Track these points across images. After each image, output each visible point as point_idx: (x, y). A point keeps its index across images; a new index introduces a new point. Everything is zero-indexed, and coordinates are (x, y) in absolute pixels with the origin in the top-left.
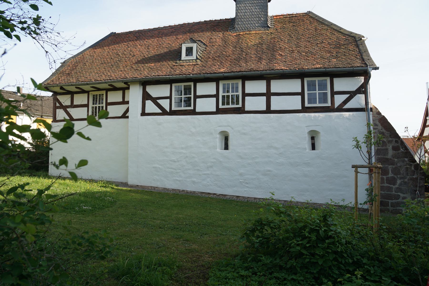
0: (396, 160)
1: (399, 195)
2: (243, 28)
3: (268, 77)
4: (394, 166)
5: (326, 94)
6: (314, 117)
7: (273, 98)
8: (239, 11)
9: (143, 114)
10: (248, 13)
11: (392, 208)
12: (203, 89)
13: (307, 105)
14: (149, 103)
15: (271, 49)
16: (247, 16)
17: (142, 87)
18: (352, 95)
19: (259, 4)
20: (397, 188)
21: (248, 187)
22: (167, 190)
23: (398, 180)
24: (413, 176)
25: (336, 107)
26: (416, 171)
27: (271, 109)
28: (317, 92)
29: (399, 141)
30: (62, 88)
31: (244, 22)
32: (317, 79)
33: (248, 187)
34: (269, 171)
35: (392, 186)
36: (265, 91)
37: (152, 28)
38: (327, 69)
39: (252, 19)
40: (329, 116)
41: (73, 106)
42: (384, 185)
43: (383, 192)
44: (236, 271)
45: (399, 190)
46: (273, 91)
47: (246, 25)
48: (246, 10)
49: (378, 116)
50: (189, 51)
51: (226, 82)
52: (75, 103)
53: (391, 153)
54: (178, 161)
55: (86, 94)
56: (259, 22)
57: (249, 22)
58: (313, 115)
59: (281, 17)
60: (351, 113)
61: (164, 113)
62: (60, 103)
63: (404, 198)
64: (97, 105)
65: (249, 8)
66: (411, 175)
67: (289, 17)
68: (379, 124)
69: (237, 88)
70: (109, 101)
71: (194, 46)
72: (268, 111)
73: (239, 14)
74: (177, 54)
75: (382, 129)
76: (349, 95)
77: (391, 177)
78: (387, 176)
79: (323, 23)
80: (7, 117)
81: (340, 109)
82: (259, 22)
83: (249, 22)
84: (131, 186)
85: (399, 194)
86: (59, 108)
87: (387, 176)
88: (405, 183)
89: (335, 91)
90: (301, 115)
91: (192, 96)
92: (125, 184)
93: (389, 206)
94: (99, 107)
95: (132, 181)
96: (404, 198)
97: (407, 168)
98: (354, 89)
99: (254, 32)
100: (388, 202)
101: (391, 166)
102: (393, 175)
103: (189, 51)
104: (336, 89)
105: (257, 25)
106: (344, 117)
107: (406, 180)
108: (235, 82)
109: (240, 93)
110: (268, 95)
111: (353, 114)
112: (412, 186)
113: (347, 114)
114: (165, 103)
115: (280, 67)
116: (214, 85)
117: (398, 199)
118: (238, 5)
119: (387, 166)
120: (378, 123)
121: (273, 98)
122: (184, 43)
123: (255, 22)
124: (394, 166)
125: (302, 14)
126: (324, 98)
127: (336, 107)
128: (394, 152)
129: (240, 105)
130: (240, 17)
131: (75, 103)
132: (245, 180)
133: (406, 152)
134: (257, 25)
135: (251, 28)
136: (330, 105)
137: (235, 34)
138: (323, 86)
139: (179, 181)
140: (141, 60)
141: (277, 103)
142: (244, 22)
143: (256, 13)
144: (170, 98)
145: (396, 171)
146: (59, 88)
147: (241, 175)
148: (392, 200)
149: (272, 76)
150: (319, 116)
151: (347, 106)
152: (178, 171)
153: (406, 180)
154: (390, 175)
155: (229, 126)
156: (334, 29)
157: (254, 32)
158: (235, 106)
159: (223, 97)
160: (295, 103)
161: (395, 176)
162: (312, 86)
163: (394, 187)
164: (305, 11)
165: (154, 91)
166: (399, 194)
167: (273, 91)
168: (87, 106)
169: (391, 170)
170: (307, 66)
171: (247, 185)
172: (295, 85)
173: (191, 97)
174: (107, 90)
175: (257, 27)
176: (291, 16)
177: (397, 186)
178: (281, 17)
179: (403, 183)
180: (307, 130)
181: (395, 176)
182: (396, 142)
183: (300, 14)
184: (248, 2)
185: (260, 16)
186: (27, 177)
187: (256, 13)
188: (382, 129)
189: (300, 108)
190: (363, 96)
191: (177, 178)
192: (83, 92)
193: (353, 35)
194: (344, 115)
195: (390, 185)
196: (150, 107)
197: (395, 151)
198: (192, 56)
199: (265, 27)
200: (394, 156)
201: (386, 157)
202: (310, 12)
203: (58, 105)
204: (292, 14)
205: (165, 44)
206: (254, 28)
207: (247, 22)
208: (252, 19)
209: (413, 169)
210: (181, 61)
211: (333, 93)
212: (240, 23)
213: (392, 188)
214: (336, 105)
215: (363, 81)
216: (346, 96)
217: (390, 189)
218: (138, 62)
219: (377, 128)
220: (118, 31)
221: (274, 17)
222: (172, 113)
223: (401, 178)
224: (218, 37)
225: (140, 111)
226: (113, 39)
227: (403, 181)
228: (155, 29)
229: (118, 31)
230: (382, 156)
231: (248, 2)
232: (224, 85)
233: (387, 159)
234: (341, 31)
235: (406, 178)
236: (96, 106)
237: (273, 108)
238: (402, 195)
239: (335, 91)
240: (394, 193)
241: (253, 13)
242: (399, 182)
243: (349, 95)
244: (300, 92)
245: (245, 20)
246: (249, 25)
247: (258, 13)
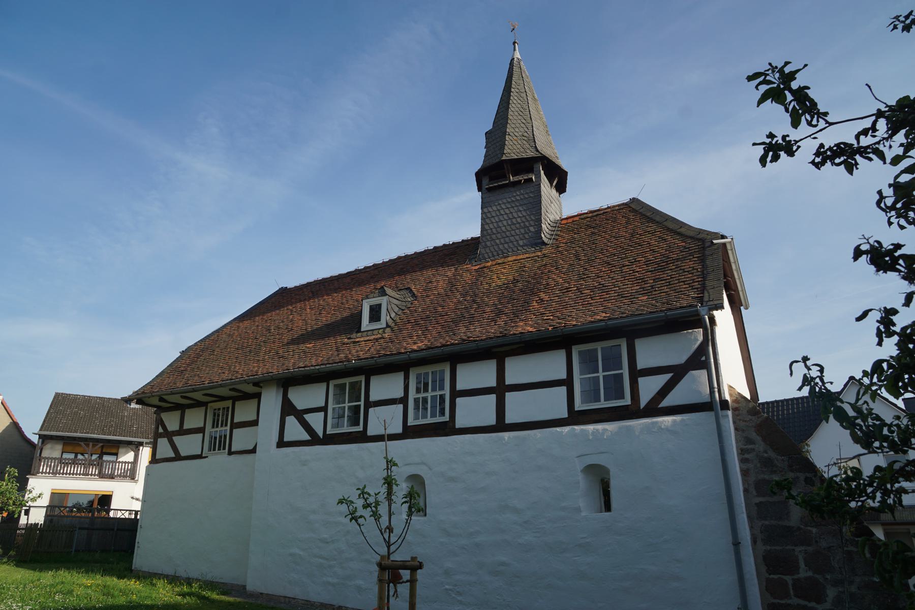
0: (814, 530)
2: (495, 253)
3: (497, 351)
6: (593, 432)
7: (509, 396)
8: (488, 221)
9: (281, 444)
12: (385, 387)
13: (579, 406)
14: (291, 420)
15: (525, 291)
16: (503, 228)
17: (282, 390)
18: (678, 373)
19: (525, 202)
25: (642, 407)
27: (457, 427)
28: (601, 374)
31: (498, 241)
32: (599, 346)
34: (503, 564)
35: (813, 604)
36: (493, 383)
37: (345, 272)
38: (610, 323)
40: (629, 428)
41: (182, 432)
42: (789, 602)
47: (501, 246)
48: (501, 218)
49: (753, 418)
50: (375, 314)
51: (422, 370)
53: (796, 514)
56: (526, 236)
57: (507, 239)
58: (590, 428)
59: (577, 219)
60: (678, 418)
61: (315, 440)
65: (507, 212)
67: (591, 217)
68: (759, 438)
69: (442, 380)
70: (460, 386)
71: (384, 301)
72: (501, 426)
74: (352, 323)
75: (766, 452)
78: (796, 577)
79: (650, 220)
81: (653, 409)
82: (526, 236)
83: (507, 239)
84: (252, 595)
87: (796, 577)
89: (639, 368)
90: (566, 429)
91: (362, 403)
92: (241, 590)
95: (253, 585)
98: (681, 358)
99: (514, 258)
101: (803, 548)
102: (810, 574)
103: (375, 314)
104: (641, 364)
105: (521, 243)
106: (660, 427)
107: (853, 589)
108: (437, 368)
109: (447, 392)
110: (501, 390)
111: (683, 420)
113: (667, 420)
114: (316, 421)
115: (526, 327)
116: (399, 378)
118: (486, 210)
119: (789, 547)
120: (754, 435)
121: (509, 396)
122: (367, 297)
123: (517, 237)
124: (810, 549)
125: (619, 205)
129: (446, 418)
131: (186, 426)
132: (456, 585)
136: (629, 403)
138: (612, 361)
140: (298, 338)
141: (518, 407)
143: (519, 220)
150: (605, 430)
151: (666, 402)
154: (804, 573)
155: (423, 463)
156: (668, 229)
157: (514, 258)
158: (439, 419)
159: (416, 401)
160: (553, 403)
162: (589, 362)
164: (625, 199)
165: (303, 398)
168: (201, 430)
170: (577, 318)
172: (552, 365)
173: (360, 405)
174: (235, 400)
175: (522, 246)
178: (577, 219)
180: (579, 466)
182: (808, 481)
183: (614, 206)
184: (505, 201)
185: (527, 224)
188: (766, 452)
189: (564, 414)
190: (704, 373)
191: (330, 579)
193: (700, 236)
194: (662, 422)
195: (806, 603)
196: (294, 430)
198: (383, 319)
199: (536, 245)
202: (634, 200)
205: (351, 302)
206: (515, 249)
208: (513, 232)
209: (868, 555)
210: (359, 334)
211: (636, 374)
212: (488, 243)
215: (701, 338)
216: (664, 378)
219: (753, 450)
220: (291, 284)
221: (564, 222)
224: (440, 278)
225: (275, 438)
231: (505, 201)
232: (418, 377)
234: (682, 230)
237: (510, 419)
239: (639, 368)
241: (514, 220)
244: (495, 385)
246: (506, 245)
247: (523, 219)
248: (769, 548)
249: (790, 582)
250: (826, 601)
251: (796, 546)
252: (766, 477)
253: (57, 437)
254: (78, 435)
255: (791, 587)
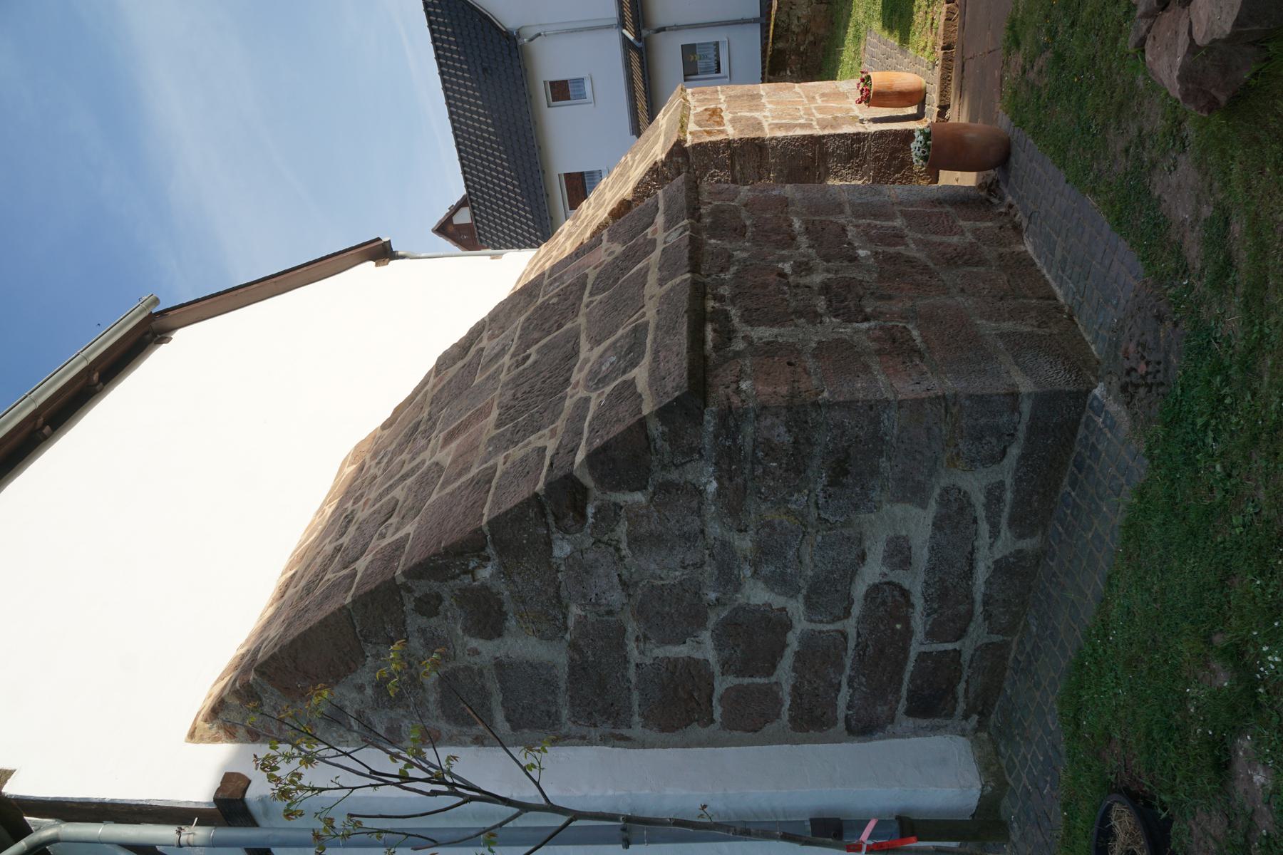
0: (575, 610)
1: (875, 588)
4: (632, 628)
11: (978, 633)
20: (810, 605)
23: (741, 599)
24: (699, 492)
26: (659, 476)
29: (423, 587)
42: (787, 688)
44: (1023, 88)
45: (827, 593)
63: (899, 553)
66: (699, 513)
75: (361, 688)
77: (719, 647)
78: (717, 669)
85: (859, 590)
88: (765, 552)
93: (958, 653)
96: (899, 553)
97: (634, 540)
100: (923, 656)
101: (631, 645)
102: (706, 636)
107: (744, 544)
112: (798, 501)
119: (632, 673)
128: (512, 623)
133: (501, 553)
145: (675, 612)
148: (908, 633)
153: (744, 544)
154: (704, 648)
161: (713, 618)
163: (801, 624)
166: (859, 590)
169: (663, 642)
177: (796, 608)
179: (766, 570)
181: (713, 618)
186: (864, 569)
188: (361, 688)
197: (503, 616)
200: (549, 621)
201: (562, 672)
213: (809, 641)
217: (819, 655)
223: (728, 580)
227: (756, 566)
230: (563, 699)
233: (578, 671)
235: (725, 545)
238: (872, 572)
240: (850, 626)
242: (757, 594)
248: (636, 718)
249: (732, 681)
250: (784, 609)
251: (626, 661)
252: (433, 697)
253: (642, 67)
254: (585, 775)
255: (747, 681)
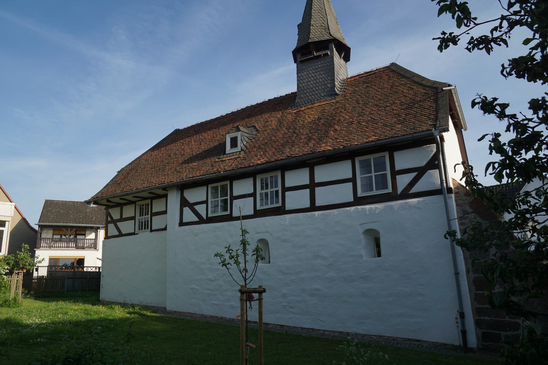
2: (306, 102)
3: (309, 163)
5: (385, 176)
6: (369, 210)
8: (301, 82)
9: (182, 224)
10: (312, 82)
12: (242, 187)
13: (360, 194)
14: (186, 210)
18: (421, 172)
21: (292, 313)
22: (205, 317)
25: (399, 193)
30: (108, 201)
31: (308, 94)
32: (372, 157)
33: (292, 313)
34: (316, 289)
39: (317, 88)
41: (122, 220)
43: (489, 318)
46: (317, 180)
49: (468, 198)
51: (264, 176)
52: (124, 216)
54: (215, 280)
55: (134, 205)
56: (326, 90)
57: (313, 93)
58: (367, 207)
59: (356, 78)
61: (201, 221)
62: (111, 217)
64: (269, 191)
69: (276, 182)
71: (239, 134)
72: (313, 208)
73: (301, 85)
74: (220, 149)
75: (475, 218)
76: (417, 173)
79: (403, 76)
80: (537, 144)
81: (406, 195)
82: (326, 90)
83: (313, 93)
84: (170, 312)
86: (110, 222)
90: (353, 208)
92: (164, 310)
94: (272, 192)
95: (170, 307)
98: (423, 163)
108: (273, 174)
110: (312, 186)
114: (201, 209)
116: (250, 181)
117: (517, 330)
118: (299, 75)
122: (229, 133)
123: (320, 91)
125: (383, 68)
126: (382, 182)
127: (399, 193)
129: (280, 204)
130: (302, 88)
132: (289, 303)
134: (322, 94)
135: (316, 99)
137: (296, 111)
138: (380, 166)
139: (217, 305)
140: (188, 160)
141: (323, 196)
142: (308, 94)
143: (320, 80)
144: (206, 202)
146: (106, 200)
147: (284, 296)
149: (315, 160)
152: (215, 292)
155: (267, 232)
160: (345, 193)
162: (366, 167)
164: (387, 64)
165: (192, 196)
167: (317, 180)
168: (133, 218)
171: (291, 310)
172: (343, 169)
174: (152, 199)
176: (368, 74)
178: (356, 78)
183: (380, 69)
184: (311, 68)
185: (326, 82)
187: (320, 80)
188: (475, 218)
191: (215, 302)
192: (130, 203)
194: (411, 202)
196: (189, 216)
198: (239, 146)
199: (332, 95)
202: (393, 64)
203: (109, 219)
204: (371, 72)
205: (219, 136)
206: (319, 99)
207: (311, 94)
208: (317, 88)
210: (225, 156)
212: (302, 96)
214: (400, 190)
218: (186, 162)
222: (210, 220)
224: (273, 119)
226: (177, 136)
228: (217, 119)
229: (181, 127)
231: (311, 68)
234: (424, 82)
236: (266, 191)
237: (318, 203)
241: (318, 81)
243: (417, 173)
245: (308, 91)
246: (313, 97)
